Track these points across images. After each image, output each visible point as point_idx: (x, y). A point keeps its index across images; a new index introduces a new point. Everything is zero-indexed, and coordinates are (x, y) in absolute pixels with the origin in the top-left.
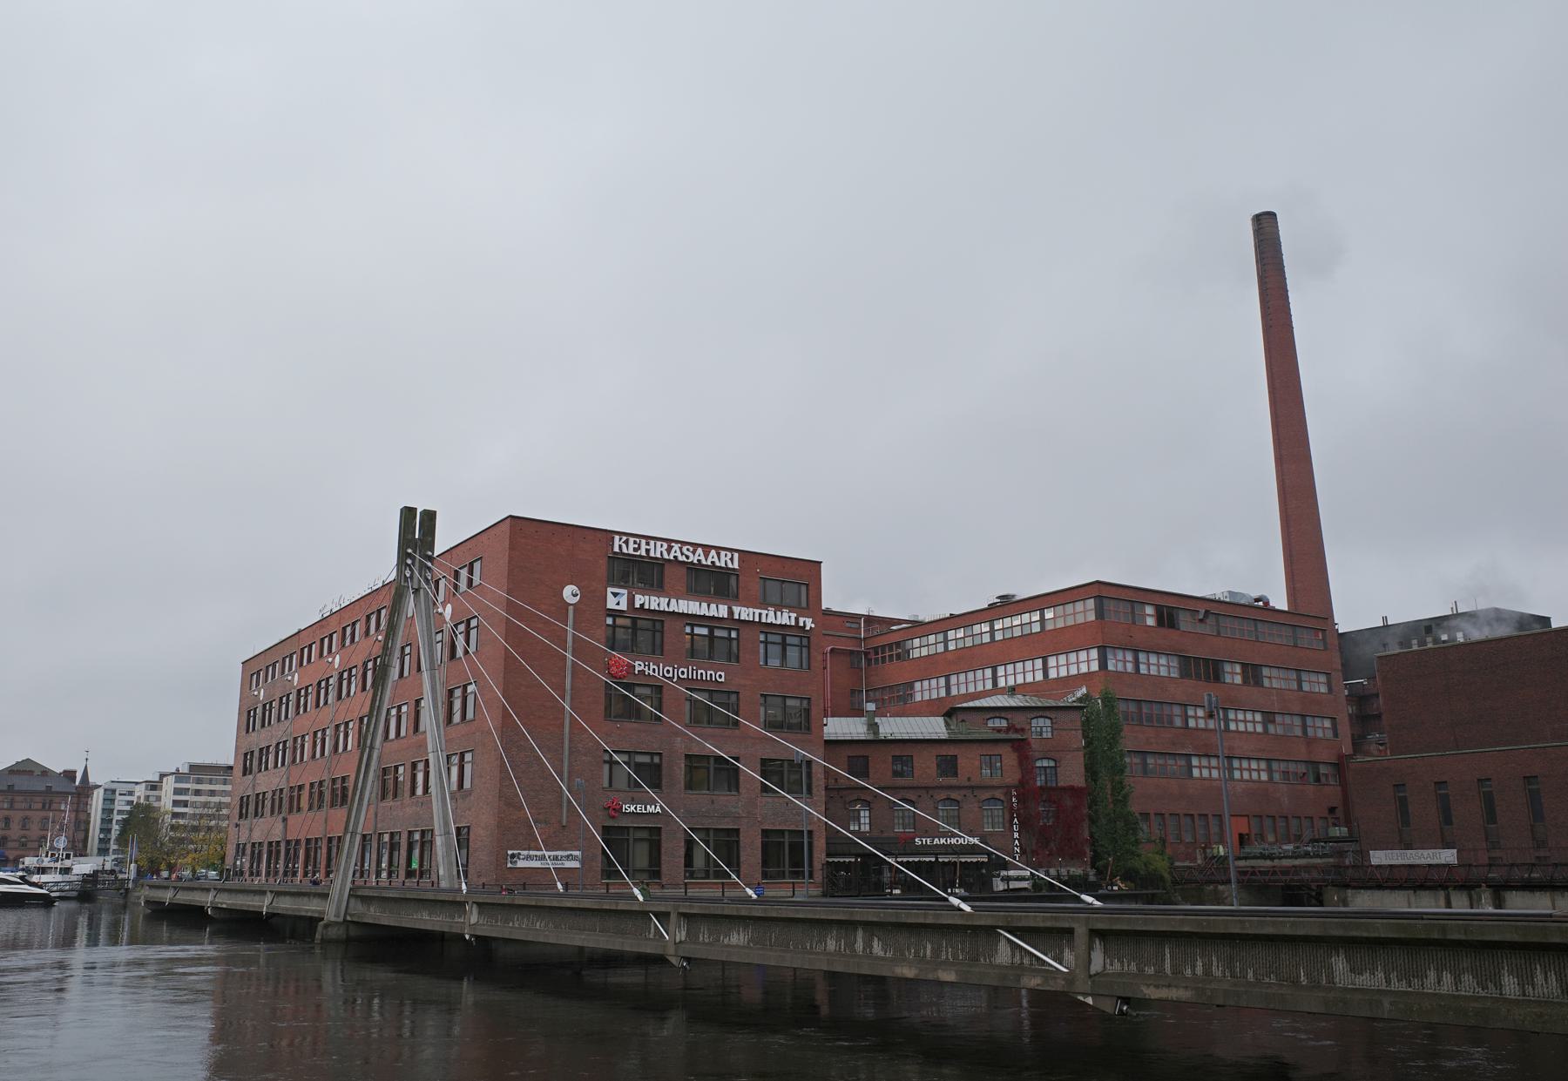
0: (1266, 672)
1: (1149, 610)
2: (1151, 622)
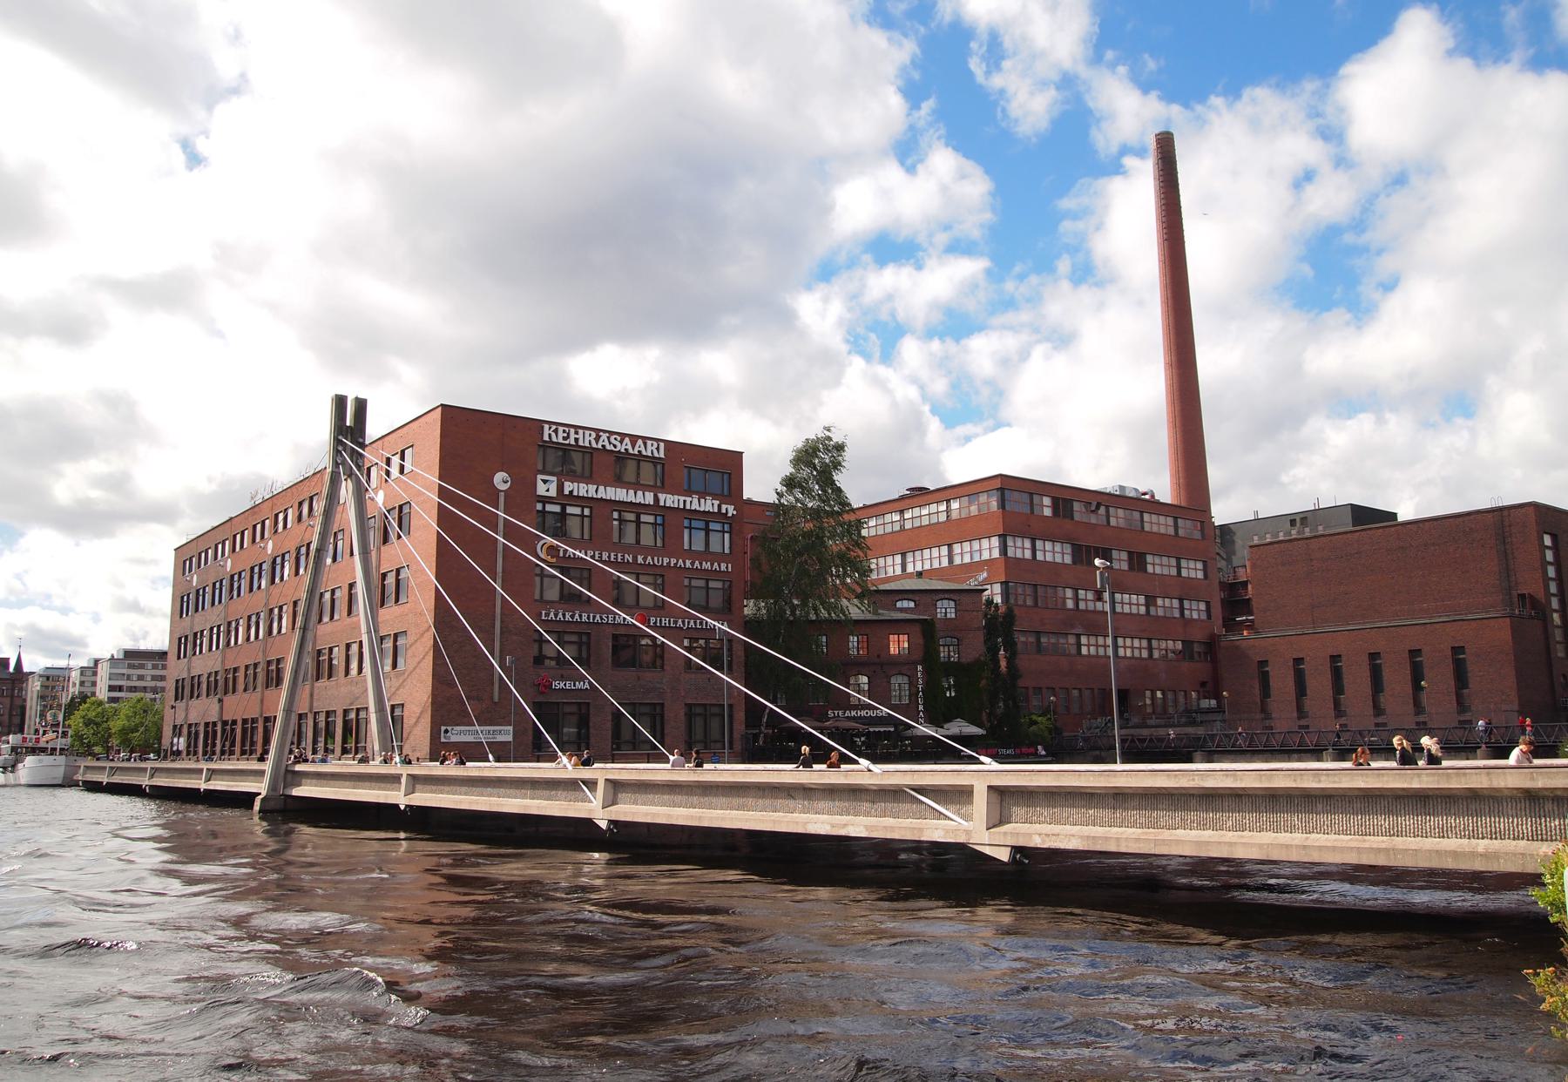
0: (1149, 558)
1: (1047, 501)
2: (1048, 512)
